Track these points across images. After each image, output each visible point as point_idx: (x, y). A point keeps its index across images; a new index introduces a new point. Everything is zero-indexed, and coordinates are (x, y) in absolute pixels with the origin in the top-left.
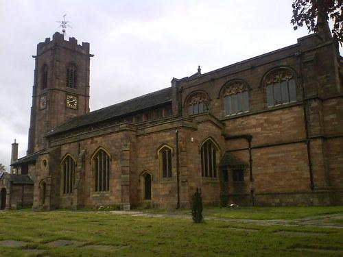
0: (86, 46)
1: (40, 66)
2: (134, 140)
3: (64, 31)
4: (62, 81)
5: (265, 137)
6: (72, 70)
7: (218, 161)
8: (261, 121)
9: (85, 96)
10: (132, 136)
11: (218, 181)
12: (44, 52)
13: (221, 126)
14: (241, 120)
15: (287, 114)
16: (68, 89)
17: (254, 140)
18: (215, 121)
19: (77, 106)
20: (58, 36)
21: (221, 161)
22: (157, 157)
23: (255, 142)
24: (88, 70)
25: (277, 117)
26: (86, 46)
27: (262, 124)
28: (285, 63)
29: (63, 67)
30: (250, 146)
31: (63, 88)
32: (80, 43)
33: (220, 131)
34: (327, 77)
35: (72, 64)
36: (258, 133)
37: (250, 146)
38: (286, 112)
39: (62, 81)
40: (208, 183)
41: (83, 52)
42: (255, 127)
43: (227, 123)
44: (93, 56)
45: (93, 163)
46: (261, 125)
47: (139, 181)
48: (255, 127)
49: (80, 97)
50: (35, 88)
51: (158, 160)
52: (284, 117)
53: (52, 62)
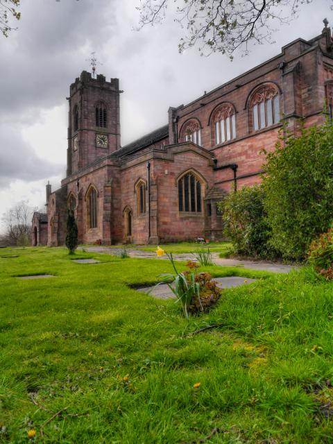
0: (115, 82)
1: (73, 107)
2: (117, 176)
3: (94, 69)
4: (91, 121)
5: (249, 166)
6: (101, 109)
7: (203, 195)
8: (247, 148)
9: (116, 135)
10: (115, 172)
11: (203, 216)
12: (75, 93)
13: (208, 155)
14: (227, 147)
15: (269, 137)
16: (97, 129)
17: (238, 169)
18: (200, 152)
19: (108, 146)
20: (85, 75)
21: (206, 195)
22: (135, 192)
23: (242, 171)
24: (117, 107)
25: (260, 142)
26: (115, 82)
27: (246, 151)
28: (269, 79)
29: (91, 106)
30: (235, 176)
31: (92, 128)
32: (108, 80)
33: (206, 162)
34: (309, 90)
35: (102, 102)
36: (243, 162)
37: (235, 176)
38: (268, 135)
39: (91, 121)
40: (187, 218)
41: (112, 88)
42: (240, 154)
43: (216, 152)
44: (122, 92)
45: (88, 199)
46: (245, 153)
47: (123, 216)
48: (240, 154)
49: (111, 136)
50: (70, 130)
51: (136, 195)
52: (267, 141)
53: (81, 101)
